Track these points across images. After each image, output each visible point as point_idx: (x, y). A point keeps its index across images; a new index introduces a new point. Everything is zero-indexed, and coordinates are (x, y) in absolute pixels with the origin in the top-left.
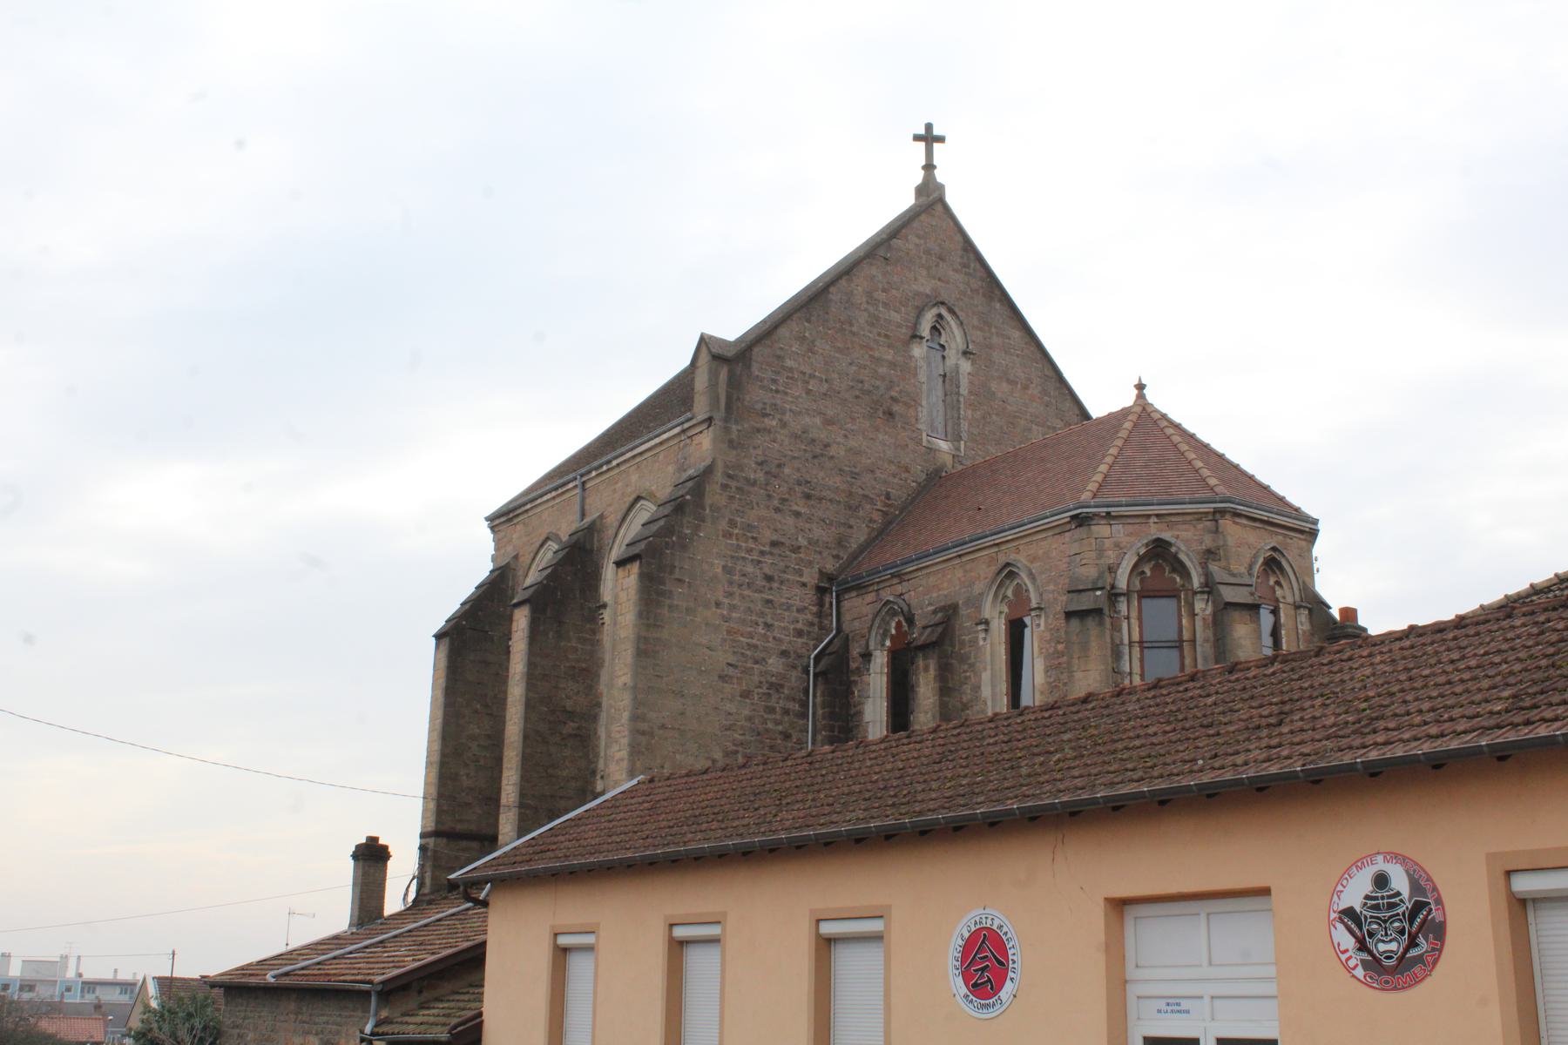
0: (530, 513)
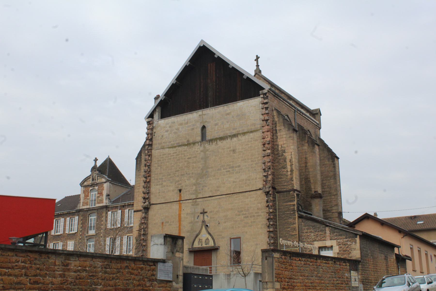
0: (280, 101)
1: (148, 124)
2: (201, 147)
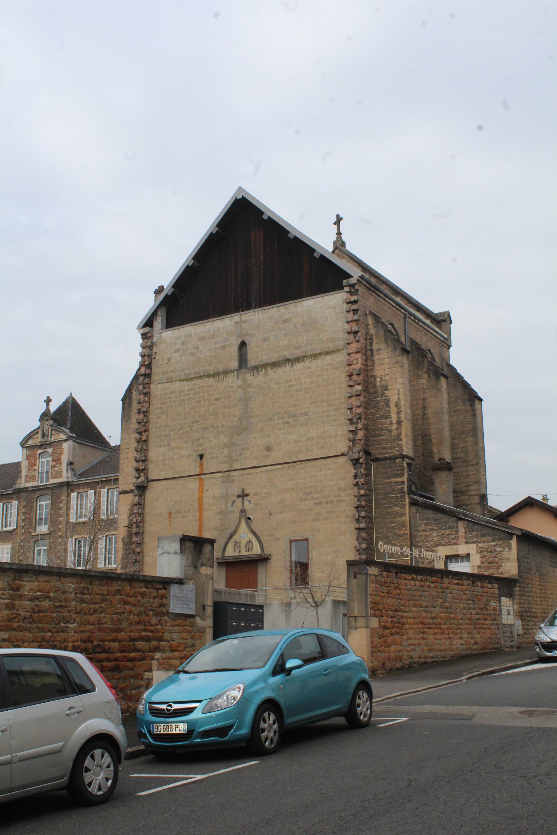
0: (379, 298)
1: (143, 339)
2: (238, 379)
